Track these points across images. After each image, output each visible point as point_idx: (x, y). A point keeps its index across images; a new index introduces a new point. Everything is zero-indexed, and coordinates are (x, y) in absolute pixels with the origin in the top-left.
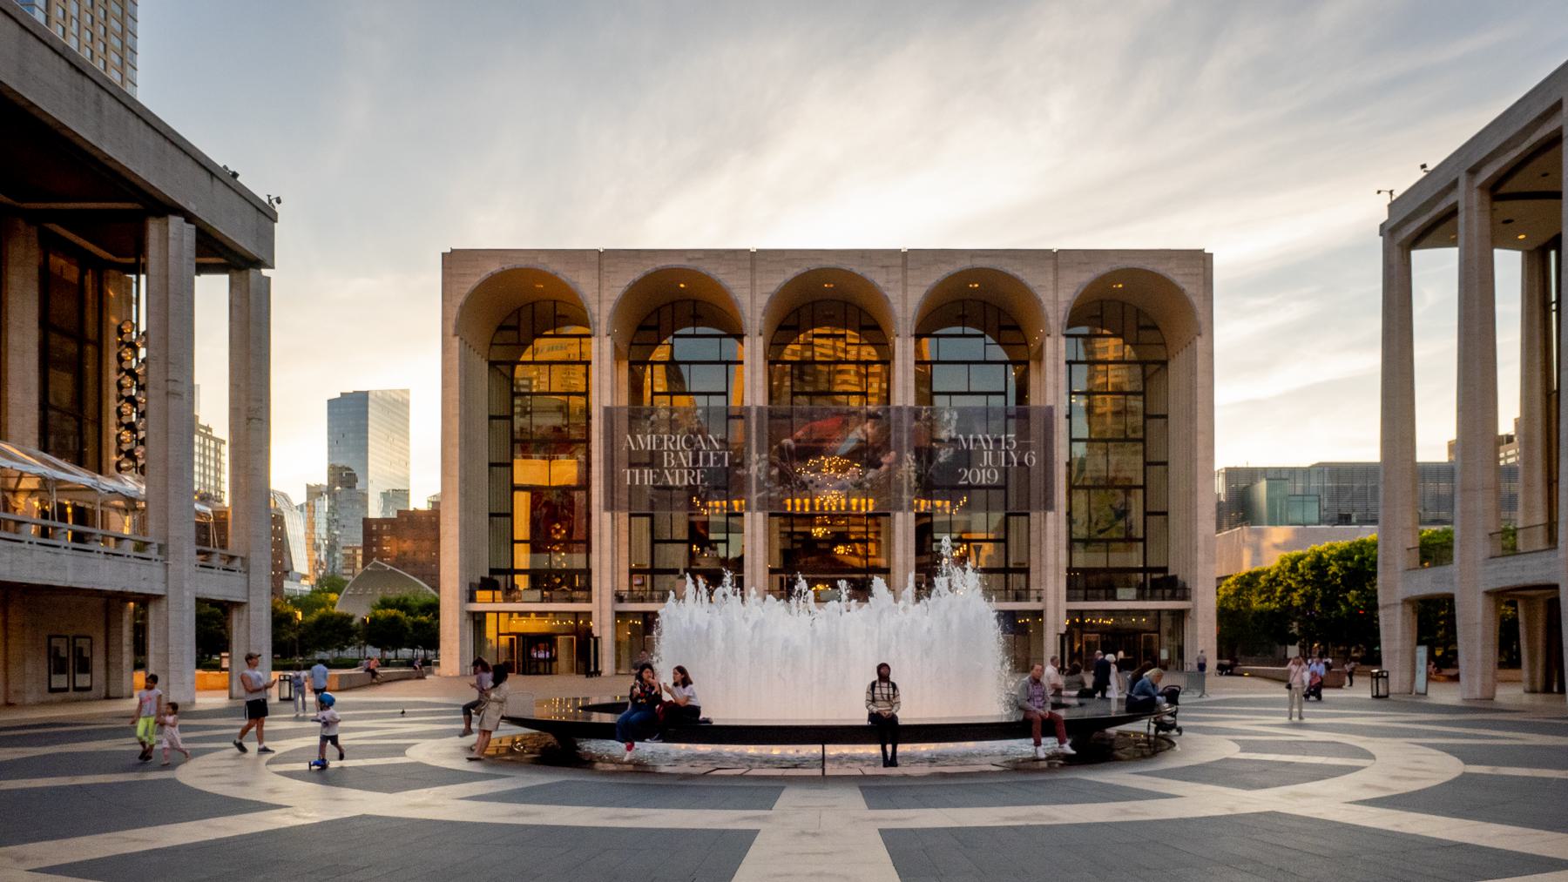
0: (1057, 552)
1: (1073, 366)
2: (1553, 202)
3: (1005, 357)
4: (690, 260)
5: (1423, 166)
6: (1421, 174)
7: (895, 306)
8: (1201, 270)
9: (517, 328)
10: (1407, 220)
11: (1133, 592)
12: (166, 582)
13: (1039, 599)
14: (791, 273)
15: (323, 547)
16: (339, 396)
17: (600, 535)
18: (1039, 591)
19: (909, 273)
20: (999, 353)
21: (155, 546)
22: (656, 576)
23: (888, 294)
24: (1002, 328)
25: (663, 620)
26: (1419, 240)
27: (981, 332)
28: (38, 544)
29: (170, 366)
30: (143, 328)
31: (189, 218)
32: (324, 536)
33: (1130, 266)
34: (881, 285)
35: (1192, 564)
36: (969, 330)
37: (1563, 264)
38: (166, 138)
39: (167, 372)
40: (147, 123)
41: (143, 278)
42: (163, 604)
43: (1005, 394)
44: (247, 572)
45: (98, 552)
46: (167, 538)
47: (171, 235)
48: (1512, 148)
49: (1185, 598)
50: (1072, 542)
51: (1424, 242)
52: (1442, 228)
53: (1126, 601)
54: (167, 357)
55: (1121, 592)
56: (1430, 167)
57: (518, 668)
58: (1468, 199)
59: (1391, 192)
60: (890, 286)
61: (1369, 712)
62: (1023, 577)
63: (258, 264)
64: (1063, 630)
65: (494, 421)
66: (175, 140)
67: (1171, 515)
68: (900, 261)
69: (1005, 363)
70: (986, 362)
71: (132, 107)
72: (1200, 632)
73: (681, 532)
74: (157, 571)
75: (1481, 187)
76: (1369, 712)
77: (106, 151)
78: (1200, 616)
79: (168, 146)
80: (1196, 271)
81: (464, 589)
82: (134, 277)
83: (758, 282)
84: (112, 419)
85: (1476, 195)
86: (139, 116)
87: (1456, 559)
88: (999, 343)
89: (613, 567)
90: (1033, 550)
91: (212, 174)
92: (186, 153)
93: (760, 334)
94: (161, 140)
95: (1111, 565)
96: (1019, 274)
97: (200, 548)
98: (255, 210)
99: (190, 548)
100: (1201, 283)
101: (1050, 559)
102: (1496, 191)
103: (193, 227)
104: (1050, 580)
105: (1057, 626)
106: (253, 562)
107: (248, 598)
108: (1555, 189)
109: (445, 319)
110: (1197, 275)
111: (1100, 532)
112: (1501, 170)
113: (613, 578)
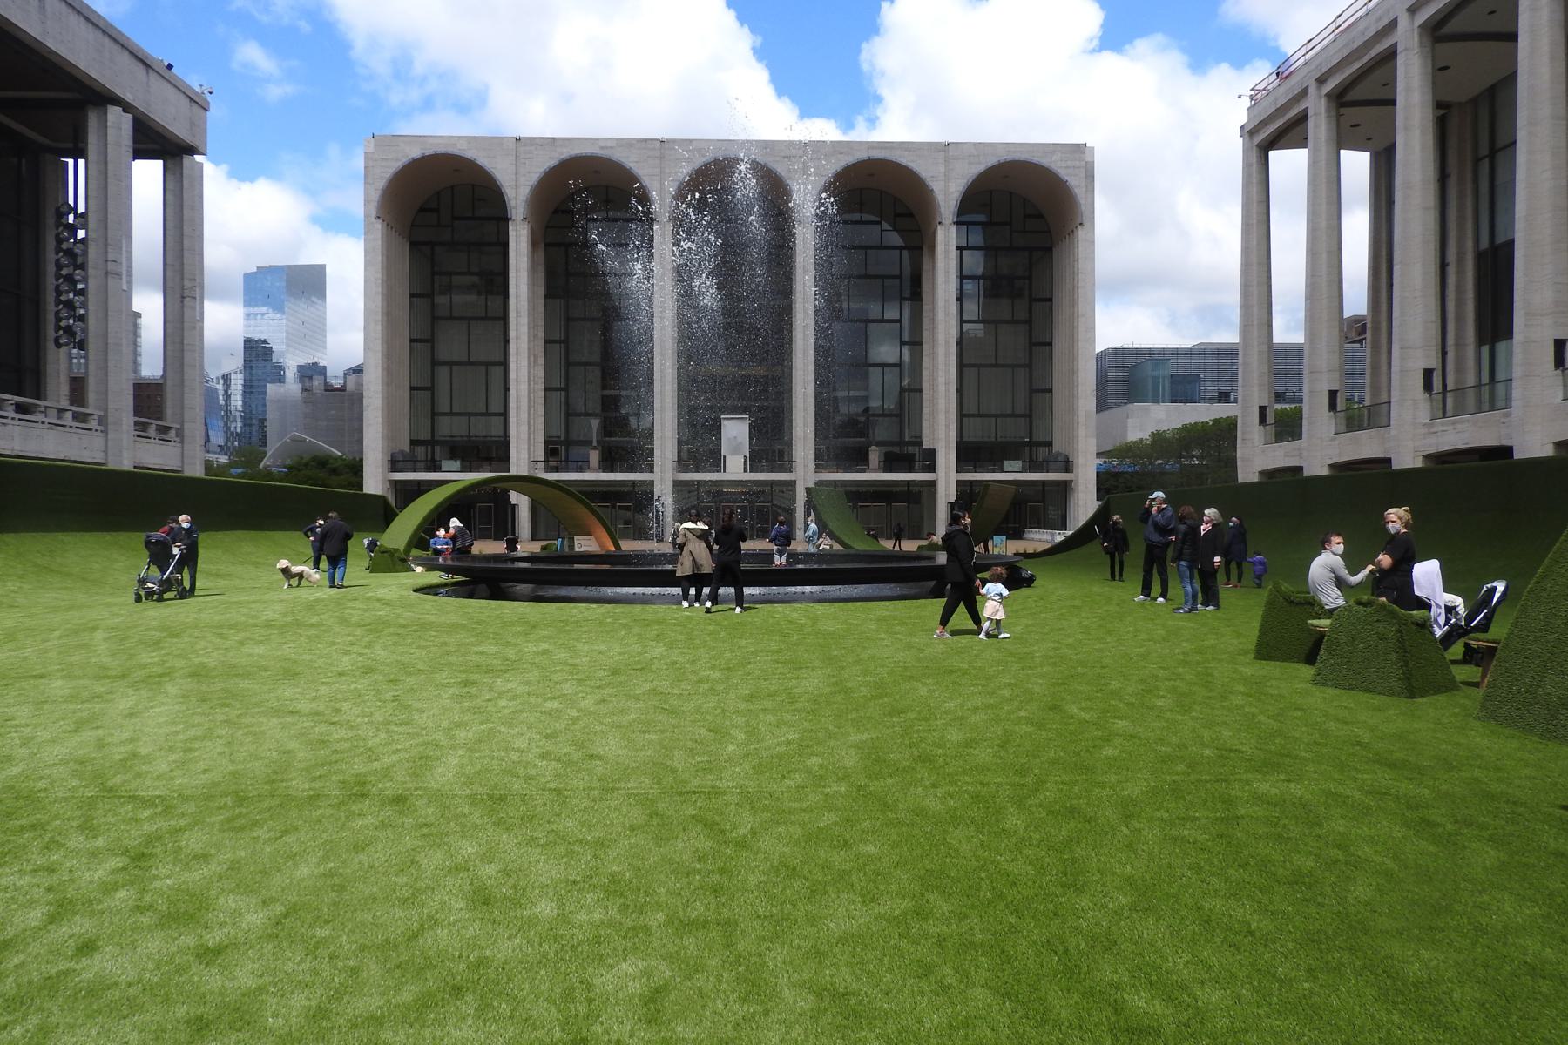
0: (947, 426)
1: (964, 252)
2: (1390, 108)
4: (602, 148)
10: (1263, 123)
11: (1018, 464)
12: (106, 452)
15: (239, 419)
16: (255, 270)
17: (518, 408)
20: (895, 239)
21: (95, 417)
24: (897, 215)
26: (1275, 142)
29: (109, 247)
30: (81, 209)
31: (127, 108)
32: (240, 408)
36: (866, 217)
38: (104, 32)
39: (106, 252)
40: (87, 19)
41: (81, 162)
43: (900, 277)
44: (182, 442)
45: (43, 423)
46: (106, 410)
47: (109, 124)
48: (1355, 61)
50: (962, 415)
51: (1282, 142)
53: (1013, 473)
54: (106, 240)
55: (446, 464)
57: (1163, 396)
58: (1318, 109)
63: (192, 150)
64: (953, 498)
65: (415, 299)
66: (114, 34)
69: (901, 248)
71: (73, 4)
72: (1081, 503)
73: (594, 404)
74: (97, 441)
75: (1328, 95)
77: (48, 45)
78: (1081, 488)
79: (107, 40)
81: (386, 459)
82: (71, 162)
84: (50, 297)
85: (1323, 101)
86: (79, 12)
87: (1304, 435)
88: (895, 230)
89: (529, 438)
91: (147, 65)
92: (122, 46)
94: (99, 34)
97: (137, 419)
98: (188, 100)
99: (128, 419)
100: (1083, 175)
102: (1340, 99)
103: (131, 116)
105: (947, 495)
106: (187, 433)
107: (182, 467)
108: (1392, 97)
109: (366, 202)
110: (1078, 168)
113: (529, 449)
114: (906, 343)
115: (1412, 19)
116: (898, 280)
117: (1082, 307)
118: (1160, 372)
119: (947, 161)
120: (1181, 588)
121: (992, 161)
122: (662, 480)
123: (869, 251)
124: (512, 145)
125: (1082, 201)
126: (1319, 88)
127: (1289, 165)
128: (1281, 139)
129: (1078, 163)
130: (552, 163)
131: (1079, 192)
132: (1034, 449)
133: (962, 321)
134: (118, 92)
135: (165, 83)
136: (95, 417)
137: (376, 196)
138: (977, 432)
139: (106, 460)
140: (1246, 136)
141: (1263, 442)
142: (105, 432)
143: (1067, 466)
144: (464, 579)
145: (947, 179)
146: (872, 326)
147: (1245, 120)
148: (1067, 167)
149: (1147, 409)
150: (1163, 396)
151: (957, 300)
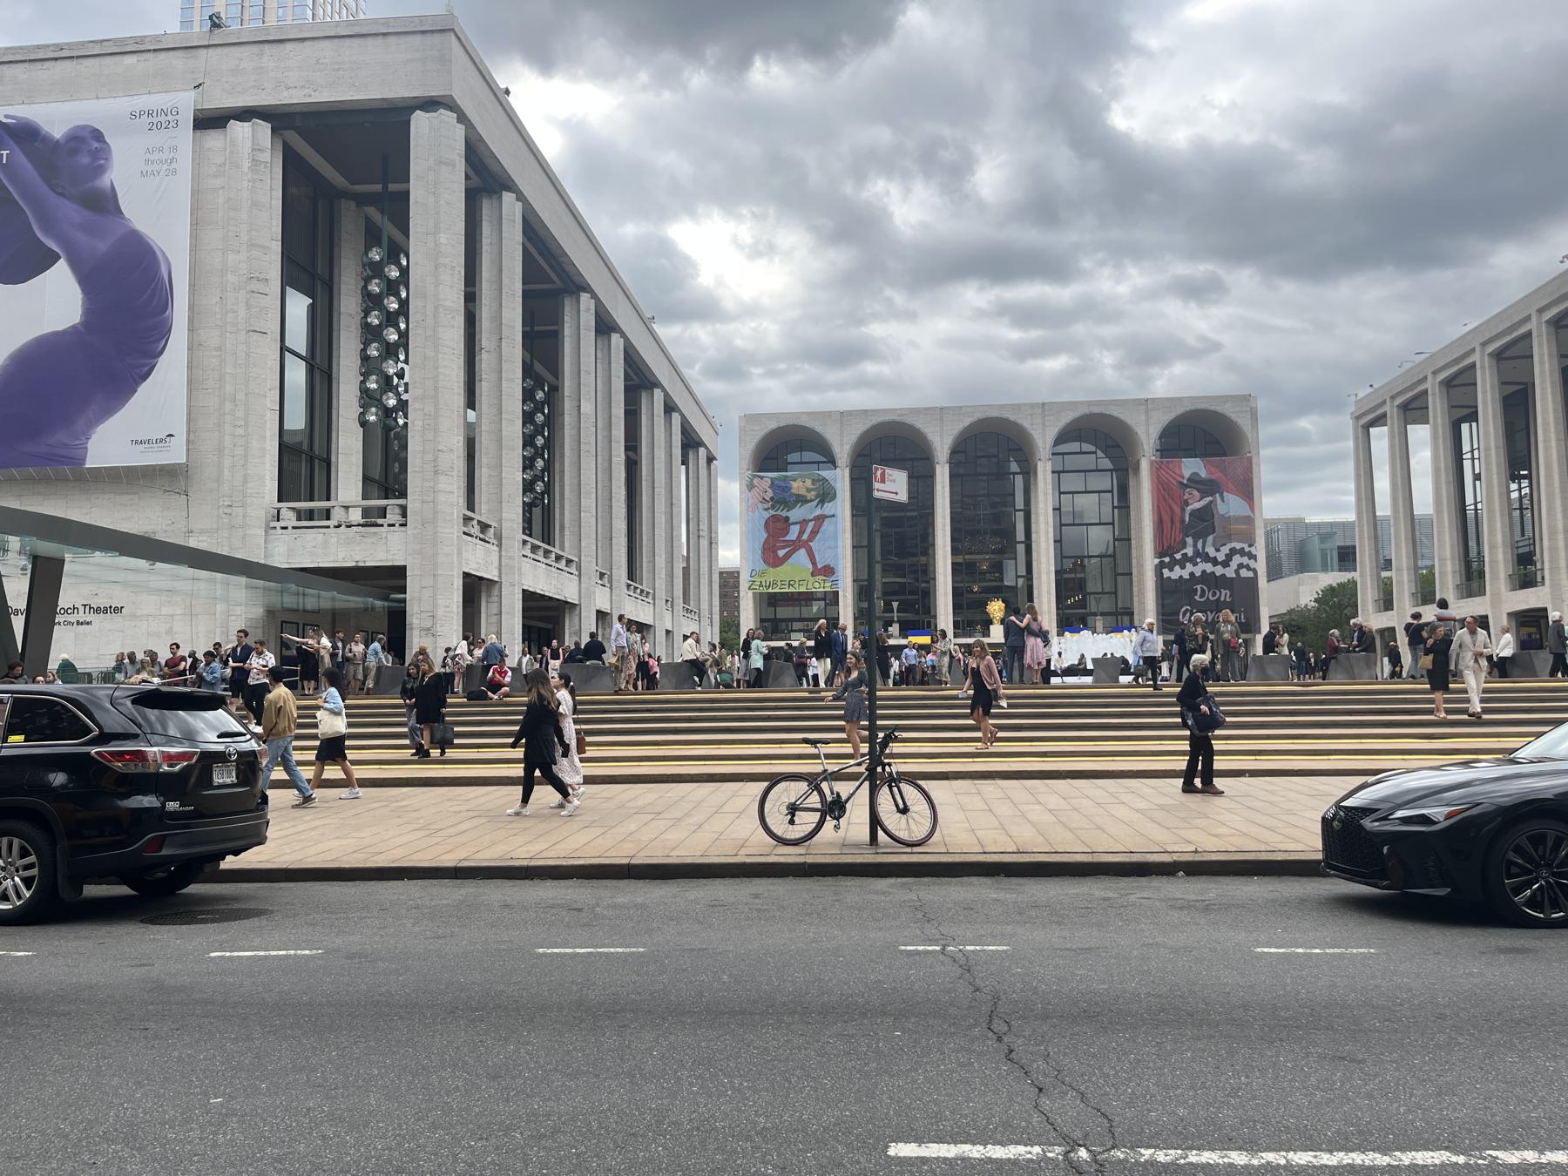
3: (1112, 467)
4: (899, 415)
5: (1371, 386)
6: (1371, 390)
7: (1038, 440)
14: (967, 422)
19: (1046, 418)
20: (1106, 463)
22: (773, 617)
23: (1032, 432)
24: (1107, 447)
25: (339, 718)
26: (1373, 423)
28: (294, 528)
33: (1199, 408)
34: (1028, 427)
39: (699, 525)
43: (1112, 491)
52: (1381, 422)
54: (699, 518)
56: (1376, 386)
57: (1332, 566)
58: (1390, 409)
59: (1356, 395)
60: (1034, 427)
61: (1489, 787)
76: (1489, 787)
82: (1228, 600)
83: (945, 428)
90: (1135, 599)
96: (1122, 417)
112: (1450, 375)
115: (1435, 378)
118: (1328, 545)
119: (1147, 412)
121: (1180, 410)
123: (1065, 456)
125: (1249, 436)
126: (1392, 402)
127: (1380, 438)
128: (1380, 420)
129: (1245, 409)
132: (1119, 617)
135: (289, 46)
136: (492, 530)
140: (1354, 420)
141: (1412, 605)
142: (500, 546)
148: (1236, 412)
149: (1317, 578)
150: (1332, 566)
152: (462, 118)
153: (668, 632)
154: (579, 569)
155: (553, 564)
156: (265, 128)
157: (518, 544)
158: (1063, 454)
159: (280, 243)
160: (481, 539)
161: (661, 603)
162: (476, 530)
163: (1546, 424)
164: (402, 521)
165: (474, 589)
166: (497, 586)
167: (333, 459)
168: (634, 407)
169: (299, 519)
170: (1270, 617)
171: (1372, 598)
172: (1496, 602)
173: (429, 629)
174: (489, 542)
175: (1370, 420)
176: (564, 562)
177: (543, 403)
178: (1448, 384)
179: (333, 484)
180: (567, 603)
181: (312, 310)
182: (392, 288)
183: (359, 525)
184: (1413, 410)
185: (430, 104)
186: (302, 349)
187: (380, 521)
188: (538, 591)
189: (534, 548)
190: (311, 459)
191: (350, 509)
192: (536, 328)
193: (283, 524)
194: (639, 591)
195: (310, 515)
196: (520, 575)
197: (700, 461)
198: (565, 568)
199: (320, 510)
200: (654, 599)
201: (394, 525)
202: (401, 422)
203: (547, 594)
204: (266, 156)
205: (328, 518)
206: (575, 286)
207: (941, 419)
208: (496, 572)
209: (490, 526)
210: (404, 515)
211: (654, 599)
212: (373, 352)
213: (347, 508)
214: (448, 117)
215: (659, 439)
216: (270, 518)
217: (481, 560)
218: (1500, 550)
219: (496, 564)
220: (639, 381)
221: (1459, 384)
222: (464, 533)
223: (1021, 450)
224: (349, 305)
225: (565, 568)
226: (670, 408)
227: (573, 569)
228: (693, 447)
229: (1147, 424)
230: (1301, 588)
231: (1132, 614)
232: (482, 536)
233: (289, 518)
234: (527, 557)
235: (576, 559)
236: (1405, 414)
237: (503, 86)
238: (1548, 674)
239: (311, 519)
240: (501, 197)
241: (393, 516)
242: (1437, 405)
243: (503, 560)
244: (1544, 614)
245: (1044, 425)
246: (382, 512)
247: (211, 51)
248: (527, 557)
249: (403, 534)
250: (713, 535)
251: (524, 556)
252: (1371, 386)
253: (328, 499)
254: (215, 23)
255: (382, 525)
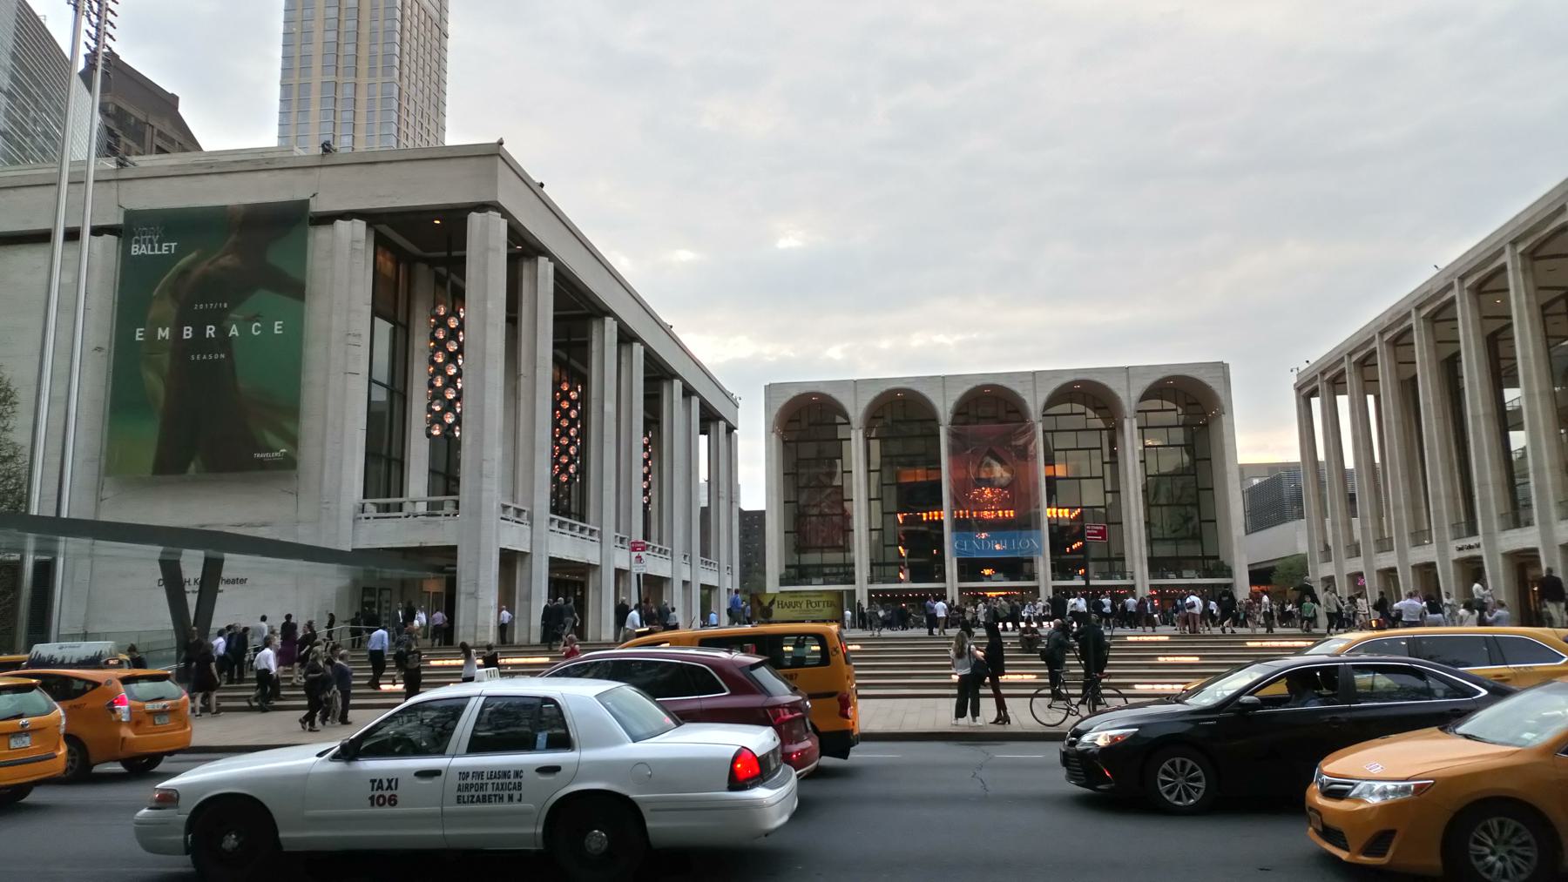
1: (1145, 430)
3: (1103, 426)
5: (1308, 362)
8: (1222, 374)
9: (799, 421)
11: (1193, 573)
13: (1132, 578)
18: (1132, 572)
20: (1099, 423)
21: (525, 514)
23: (1024, 397)
27: (1174, 407)
28: (375, 518)
35: (1231, 555)
36: (1168, 405)
37: (58, 470)
42: (717, 591)
44: (601, 542)
49: (1230, 576)
50: (1151, 541)
55: (814, 581)
56: (1312, 362)
62: (1120, 563)
66: (646, 307)
67: (1218, 521)
68: (1031, 378)
69: (1100, 430)
70: (1168, 427)
75: (1327, 381)
80: (1219, 375)
83: (947, 394)
93: (773, 432)
95: (1180, 555)
101: (1136, 552)
104: (1137, 566)
111: (1174, 531)
114: (1106, 463)
116: (1101, 480)
117: (1226, 441)
120: (54, 657)
122: (861, 589)
124: (1037, 504)
128: (1314, 393)
130: (877, 394)
131: (1220, 392)
132: (1206, 561)
133: (1147, 476)
134: (725, 416)
135: (380, 166)
136: (525, 514)
137: (773, 418)
138: (1164, 550)
139: (531, 549)
142: (531, 525)
143: (1228, 572)
144: (192, 617)
145: (856, 409)
146: (1082, 481)
147: (1296, 381)
151: (1141, 462)
152: (505, 214)
153: (685, 583)
154: (601, 536)
155: (578, 535)
156: (360, 226)
157: (546, 523)
158: (1146, 411)
159: (370, 307)
160: (516, 522)
161: (679, 558)
162: (511, 514)
163: (1427, 404)
164: (455, 511)
165: (510, 559)
166: (529, 556)
167: (406, 459)
168: (656, 392)
169: (378, 512)
170: (1249, 566)
171: (1555, 496)
172: (1339, 567)
173: (473, 594)
174: (522, 523)
175: (1305, 393)
176: (587, 532)
177: (577, 401)
178: (1479, 290)
179: (405, 478)
180: (589, 564)
181: (394, 333)
182: (453, 334)
183: (423, 515)
184: (1336, 384)
185: (482, 207)
186: (384, 379)
187: (439, 512)
188: (565, 558)
189: (561, 524)
190: (389, 462)
191: (417, 504)
192: (573, 339)
193: (366, 515)
194: (657, 550)
195: (387, 508)
196: (547, 547)
197: (720, 433)
198: (588, 537)
199: (395, 504)
200: (672, 555)
201: (449, 515)
202: (457, 434)
203: (572, 559)
204: (361, 246)
205: (401, 511)
206: (601, 312)
207: (944, 387)
208: (528, 546)
209: (524, 511)
210: (457, 507)
211: (672, 555)
212: (441, 335)
213: (415, 502)
214: (494, 216)
215: (678, 415)
216: (357, 510)
217: (514, 537)
218: (1491, 488)
219: (528, 538)
220: (658, 374)
221: (1366, 363)
222: (502, 518)
223: (1017, 411)
224: (421, 344)
225: (588, 537)
226: (688, 392)
227: (668, 556)
228: (667, 379)
229: (1129, 389)
230: (1298, 533)
231: (1123, 559)
232: (517, 519)
233: (371, 510)
234: (554, 531)
235: (598, 529)
236: (1433, 326)
237: (538, 181)
238: (1475, 622)
239: (388, 511)
240: (537, 261)
241: (449, 509)
242: (1351, 379)
243: (534, 536)
244: (1535, 554)
245: (1035, 392)
246: (440, 505)
247: (323, 170)
248: (554, 531)
249: (455, 520)
250: (733, 495)
251: (551, 531)
252: (1308, 362)
253: (401, 496)
254: (327, 148)
255: (440, 515)
